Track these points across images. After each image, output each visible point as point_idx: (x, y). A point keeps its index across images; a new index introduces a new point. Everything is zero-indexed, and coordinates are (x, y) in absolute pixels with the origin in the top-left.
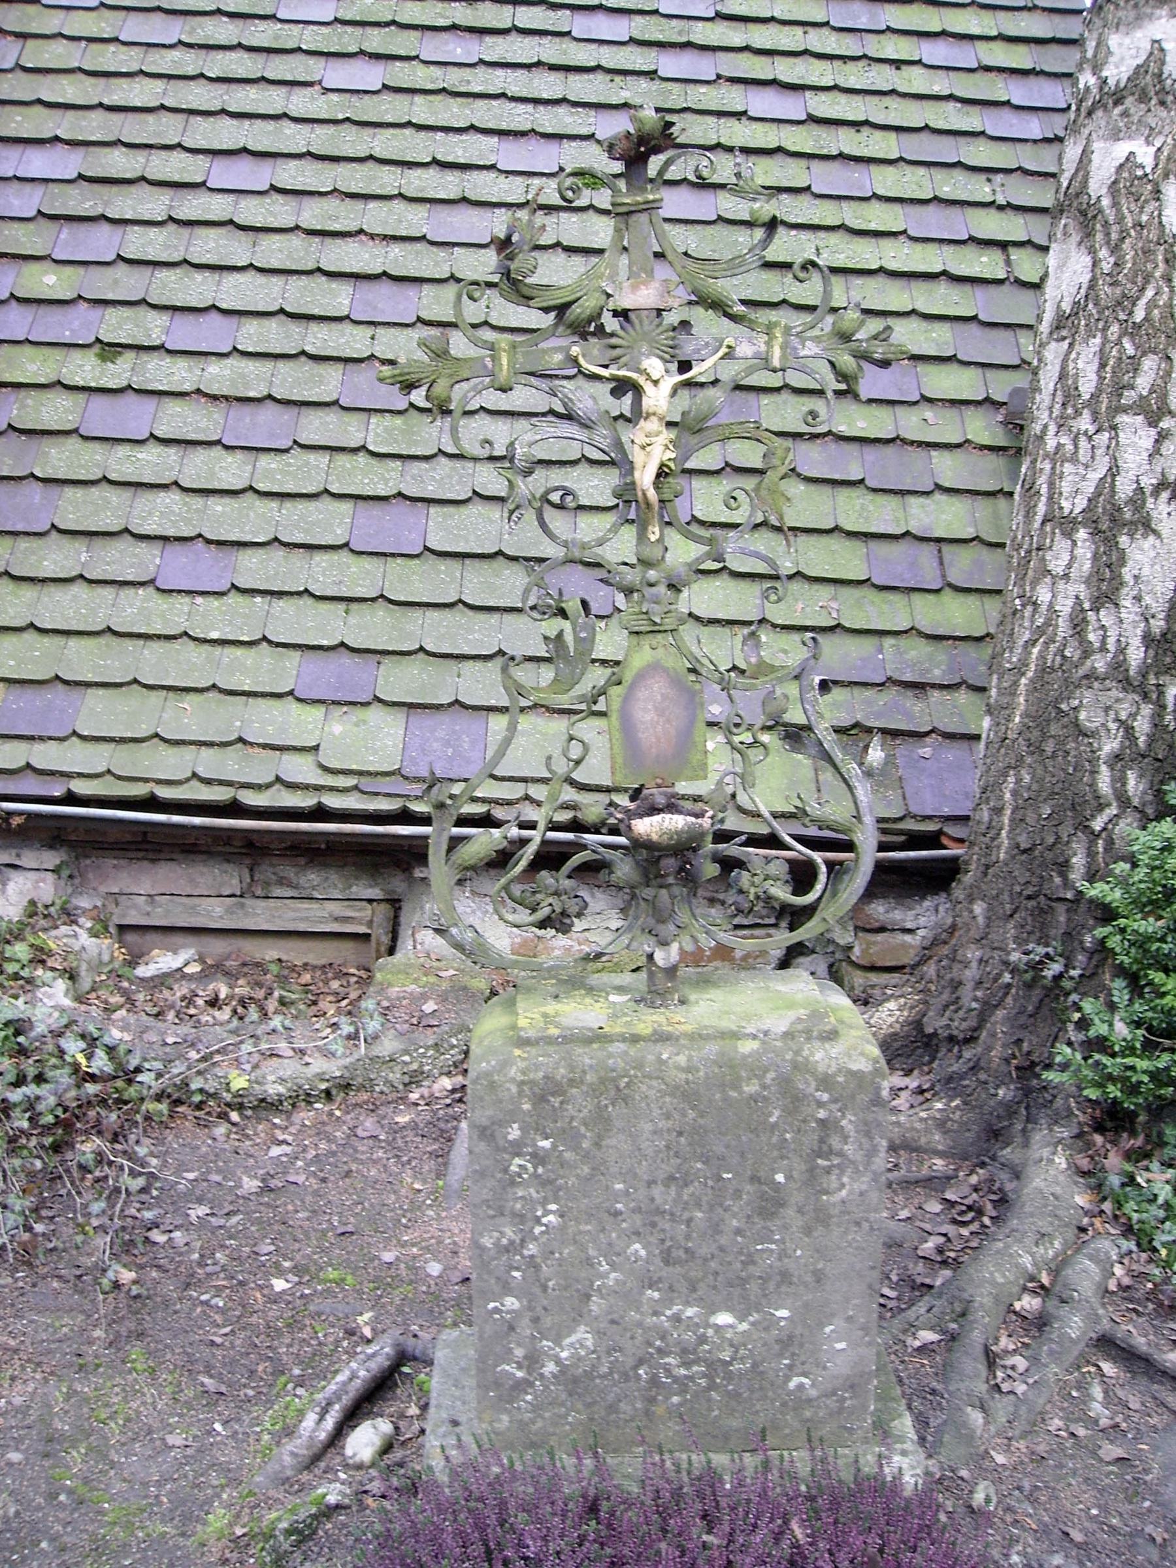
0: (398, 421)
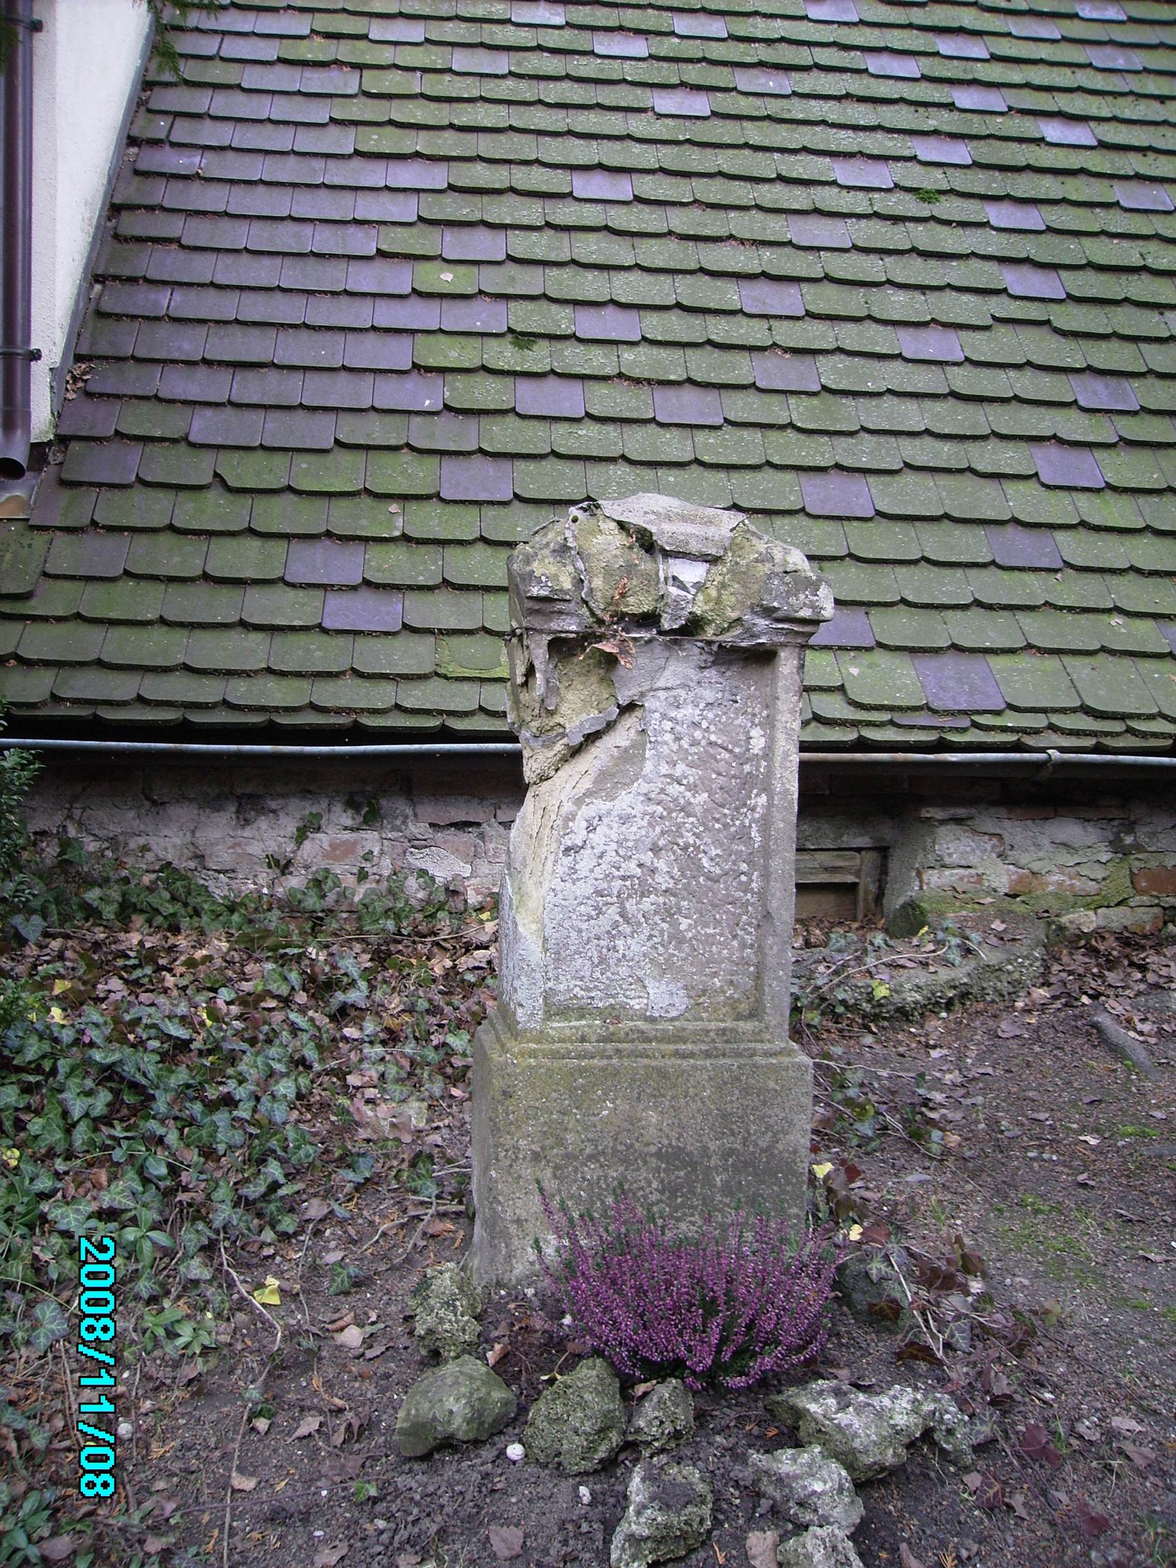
0: (815, 401)
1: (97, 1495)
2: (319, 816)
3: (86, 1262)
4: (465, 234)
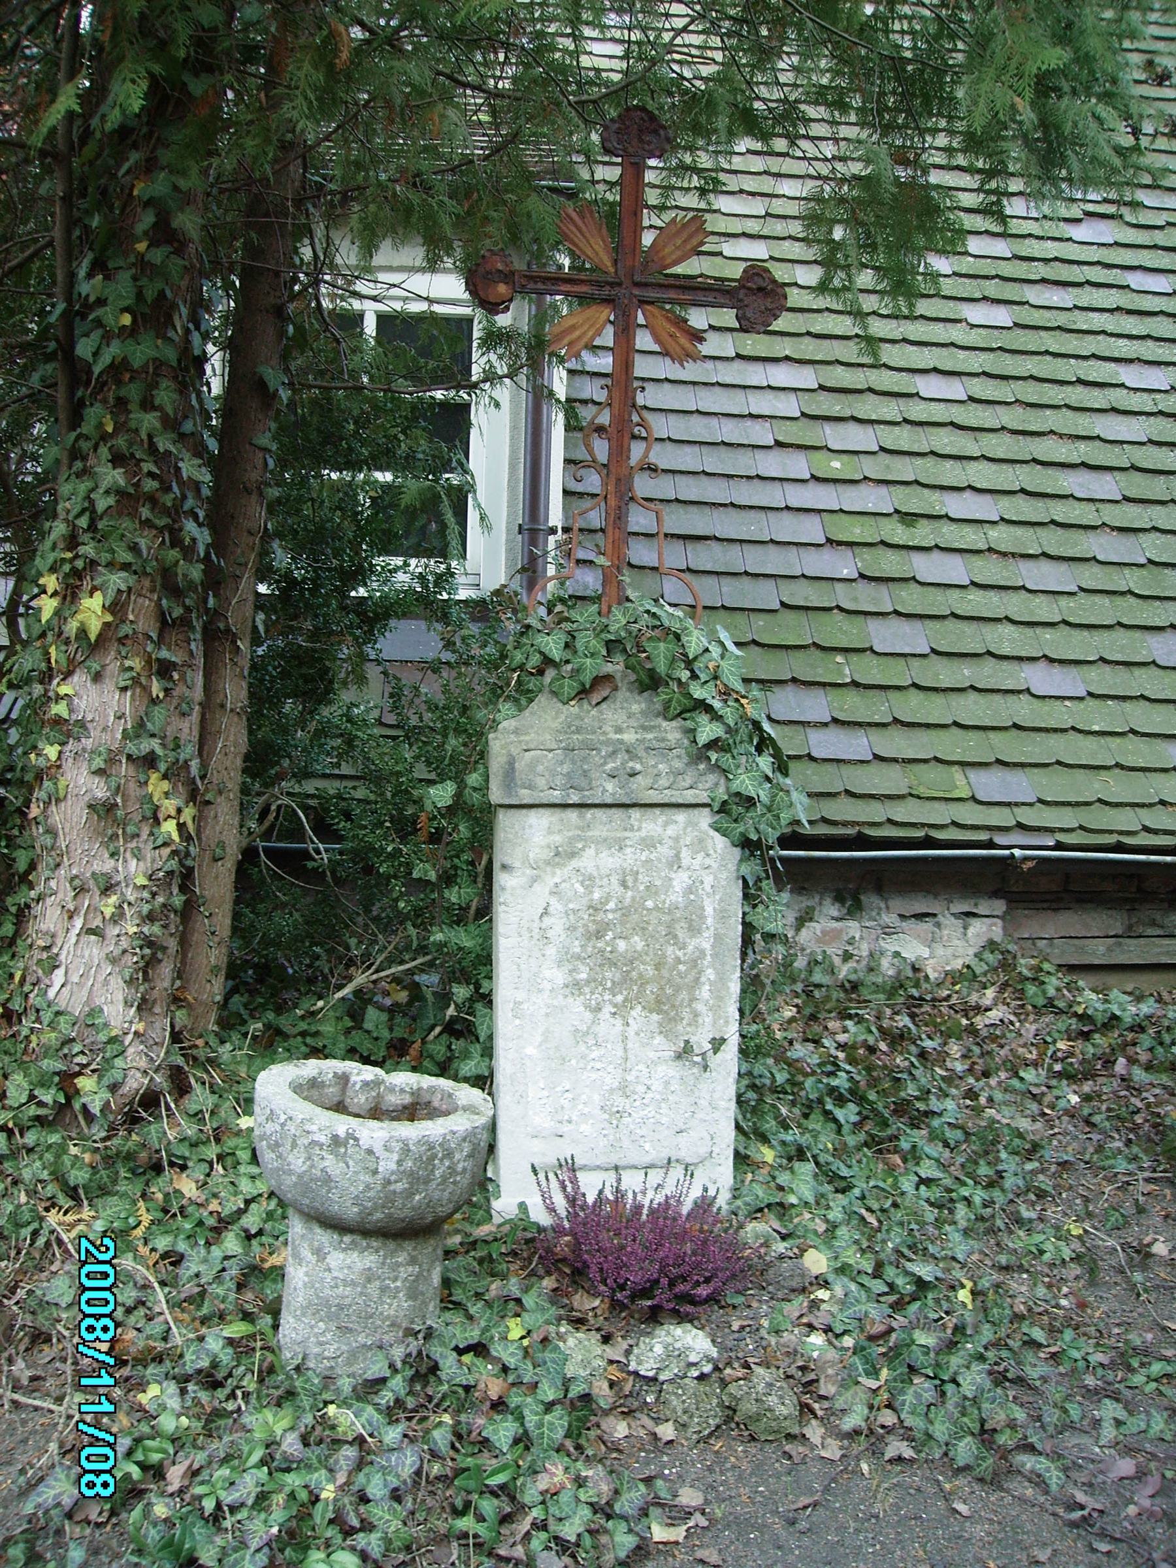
0: (1144, 572)
1: (97, 1494)
2: (813, 909)
3: (84, 1263)
4: (841, 427)
